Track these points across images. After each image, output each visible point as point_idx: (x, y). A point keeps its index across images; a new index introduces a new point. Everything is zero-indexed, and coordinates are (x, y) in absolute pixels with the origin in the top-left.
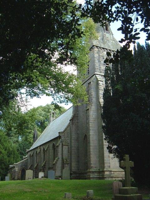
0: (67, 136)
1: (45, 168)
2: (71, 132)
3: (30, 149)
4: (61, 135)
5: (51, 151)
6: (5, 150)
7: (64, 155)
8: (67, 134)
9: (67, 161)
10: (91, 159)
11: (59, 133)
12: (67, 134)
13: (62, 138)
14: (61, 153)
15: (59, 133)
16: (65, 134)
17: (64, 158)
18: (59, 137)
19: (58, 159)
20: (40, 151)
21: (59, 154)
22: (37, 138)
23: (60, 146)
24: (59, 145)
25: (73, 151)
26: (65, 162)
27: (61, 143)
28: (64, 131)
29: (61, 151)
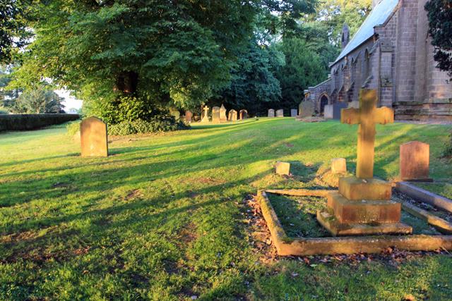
0: (392, 33)
1: (352, 94)
2: (400, 23)
3: (337, 60)
4: (378, 32)
5: (363, 58)
6: (301, 65)
7: (382, 71)
8: (392, 29)
9: (388, 82)
10: (433, 78)
11: (374, 28)
12: (392, 29)
13: (381, 38)
14: (377, 68)
15: (346, 158)
16: (386, 29)
17: (383, 75)
18: (376, 36)
19: (372, 78)
20: (347, 64)
21: (373, 68)
22: (348, 40)
23: (377, 54)
24: (375, 51)
25: (402, 71)
26: (383, 85)
27: (378, 49)
28: (385, 23)
29: (377, 63)
